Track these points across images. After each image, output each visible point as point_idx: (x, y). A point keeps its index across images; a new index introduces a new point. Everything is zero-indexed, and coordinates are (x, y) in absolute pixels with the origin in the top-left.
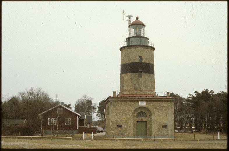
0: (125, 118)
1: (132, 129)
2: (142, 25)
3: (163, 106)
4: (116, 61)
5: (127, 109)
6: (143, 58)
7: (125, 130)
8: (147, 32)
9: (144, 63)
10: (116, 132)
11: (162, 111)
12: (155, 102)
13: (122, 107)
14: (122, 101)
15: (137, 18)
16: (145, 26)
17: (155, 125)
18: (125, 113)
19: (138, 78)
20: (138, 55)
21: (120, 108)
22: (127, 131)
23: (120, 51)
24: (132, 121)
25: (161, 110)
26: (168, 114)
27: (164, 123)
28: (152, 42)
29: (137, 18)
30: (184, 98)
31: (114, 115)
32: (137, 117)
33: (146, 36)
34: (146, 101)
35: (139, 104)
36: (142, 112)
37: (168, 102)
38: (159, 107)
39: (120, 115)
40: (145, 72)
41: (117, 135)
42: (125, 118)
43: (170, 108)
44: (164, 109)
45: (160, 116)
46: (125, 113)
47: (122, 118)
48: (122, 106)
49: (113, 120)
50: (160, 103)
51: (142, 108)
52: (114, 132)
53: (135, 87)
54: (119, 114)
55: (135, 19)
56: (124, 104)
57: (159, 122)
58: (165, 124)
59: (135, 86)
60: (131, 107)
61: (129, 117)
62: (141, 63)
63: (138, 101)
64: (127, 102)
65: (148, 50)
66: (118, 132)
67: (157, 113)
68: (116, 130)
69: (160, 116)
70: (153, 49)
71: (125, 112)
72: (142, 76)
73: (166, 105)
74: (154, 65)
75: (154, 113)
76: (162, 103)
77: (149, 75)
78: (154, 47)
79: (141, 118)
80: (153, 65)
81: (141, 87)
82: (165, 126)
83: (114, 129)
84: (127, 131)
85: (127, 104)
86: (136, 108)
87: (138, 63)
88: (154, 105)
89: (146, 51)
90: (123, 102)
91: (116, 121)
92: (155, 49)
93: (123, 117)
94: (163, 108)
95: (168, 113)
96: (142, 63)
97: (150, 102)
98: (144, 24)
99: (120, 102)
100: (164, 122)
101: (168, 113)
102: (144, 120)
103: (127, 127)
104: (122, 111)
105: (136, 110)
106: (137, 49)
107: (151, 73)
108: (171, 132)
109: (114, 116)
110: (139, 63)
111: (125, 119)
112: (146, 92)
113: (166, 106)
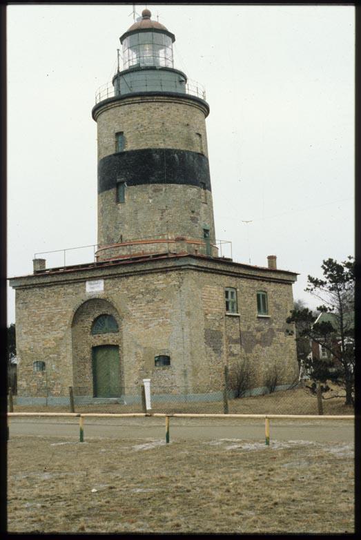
1: (71, 374)
6: (127, 136)
7: (52, 377)
9: (132, 151)
10: (31, 384)
11: (151, 307)
12: (131, 279)
14: (44, 287)
16: (172, 37)
17: (133, 359)
19: (114, 203)
20: (113, 131)
22: (58, 381)
24: (70, 347)
25: (148, 302)
26: (171, 314)
27: (160, 347)
28: (200, 87)
31: (25, 333)
32: (92, 333)
33: (177, 67)
34: (104, 277)
36: (104, 315)
37: (170, 273)
38: (142, 293)
40: (133, 182)
41: (36, 395)
43: (175, 293)
44: (155, 300)
45: (146, 326)
47: (43, 340)
48: (43, 302)
49: (23, 349)
50: (144, 281)
51: (94, 302)
52: (27, 384)
54: (36, 329)
57: (144, 345)
58: (163, 354)
60: (66, 301)
61: (61, 335)
62: (122, 154)
63: (84, 280)
64: (56, 289)
65: (147, 105)
66: (36, 384)
67: (138, 315)
68: (33, 378)
69: (146, 326)
70: (204, 108)
71: (50, 320)
72: (125, 197)
73: (164, 286)
75: (129, 315)
76: (150, 278)
77: (150, 187)
78: (208, 101)
79: (104, 335)
80: (202, 158)
81: (121, 233)
82: (165, 360)
83: (26, 375)
84: (58, 381)
85: (55, 292)
86: (80, 302)
87: (153, 159)
88: (127, 289)
89: (139, 112)
90: (45, 289)
91: (30, 349)
93: (48, 337)
94: (155, 296)
95: (171, 311)
96: (124, 152)
99: (37, 289)
100: (161, 345)
101: (171, 311)
102: (111, 342)
103: (58, 367)
104: (43, 319)
105: (79, 313)
106: (112, 111)
107: (193, 182)
108: (183, 379)
110: (115, 155)
111: (52, 344)
112: (137, 246)
113: (161, 287)
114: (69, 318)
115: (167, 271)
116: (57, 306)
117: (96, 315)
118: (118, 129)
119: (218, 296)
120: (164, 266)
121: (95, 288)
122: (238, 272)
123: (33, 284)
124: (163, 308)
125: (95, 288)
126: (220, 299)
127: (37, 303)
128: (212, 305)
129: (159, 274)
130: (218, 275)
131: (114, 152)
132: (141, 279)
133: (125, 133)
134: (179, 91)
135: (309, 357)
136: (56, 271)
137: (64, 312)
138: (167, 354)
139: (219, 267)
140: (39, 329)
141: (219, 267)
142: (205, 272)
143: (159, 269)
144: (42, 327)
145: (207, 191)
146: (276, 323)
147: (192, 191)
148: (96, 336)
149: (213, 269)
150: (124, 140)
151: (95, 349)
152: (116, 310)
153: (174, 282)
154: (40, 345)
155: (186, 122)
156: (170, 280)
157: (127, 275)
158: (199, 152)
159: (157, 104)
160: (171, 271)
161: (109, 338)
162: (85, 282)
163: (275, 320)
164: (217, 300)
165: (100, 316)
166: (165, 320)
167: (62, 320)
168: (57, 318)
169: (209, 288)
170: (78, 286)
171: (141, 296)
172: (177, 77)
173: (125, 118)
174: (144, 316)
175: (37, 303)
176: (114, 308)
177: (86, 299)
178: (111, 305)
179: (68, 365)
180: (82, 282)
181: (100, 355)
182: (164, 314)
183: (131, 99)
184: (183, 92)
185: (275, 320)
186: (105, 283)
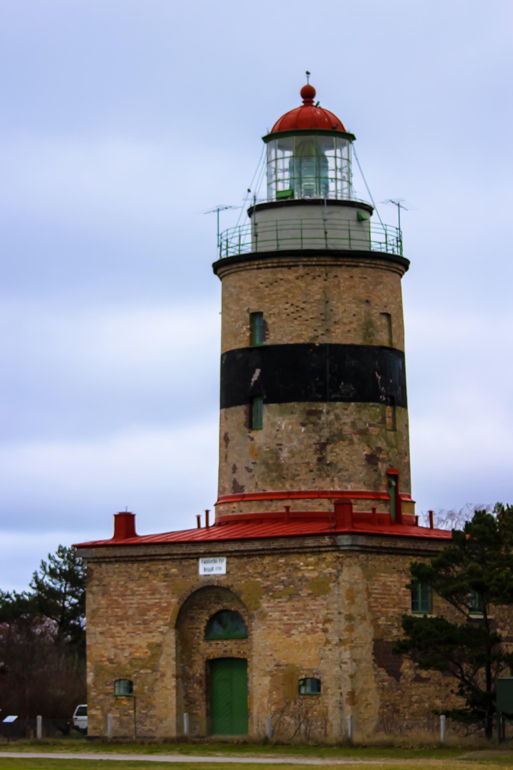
0: (142, 641)
2: (335, 132)
3: (300, 574)
4: (191, 334)
5: (150, 602)
6: (269, 321)
8: (363, 173)
13: (133, 593)
15: (308, 94)
18: (145, 622)
21: (123, 595)
23: (216, 278)
27: (307, 665)
29: (308, 94)
30: (74, 546)
31: (102, 633)
34: (228, 554)
35: (197, 572)
37: (324, 555)
38: (282, 582)
39: (123, 633)
42: (144, 645)
46: (145, 622)
47: (131, 646)
51: (211, 589)
53: (235, 482)
54: (119, 629)
55: (298, 102)
56: (140, 577)
59: (235, 476)
61: (157, 639)
63: (197, 556)
67: (276, 615)
69: (288, 633)
70: (399, 264)
74: (401, 355)
75: (263, 616)
78: (405, 255)
92: (407, 268)
93: (137, 641)
97: (245, 560)
98: (348, 128)
109: (101, 639)
114: (170, 613)
115: (320, 552)
116: (153, 594)
117: (213, 611)
118: (254, 307)
119: (399, 589)
120: (316, 544)
121: (212, 568)
122: (435, 549)
123: (115, 557)
124: (313, 608)
125: (212, 568)
126: (401, 593)
127: (122, 586)
128: (388, 603)
129: (308, 555)
130: (399, 557)
131: (244, 344)
132: (282, 560)
133: (265, 314)
134: (357, 246)
135: (51, 599)
136: (152, 543)
137: (166, 605)
138: (316, 676)
139: (400, 544)
140: (123, 629)
141: (400, 544)
142: (379, 553)
143: (308, 547)
144: (130, 627)
145: (399, 408)
146: (502, 629)
147: (368, 414)
148: (214, 642)
149: (390, 548)
150: (264, 327)
151: (212, 664)
152: (244, 606)
153: (330, 570)
154: (126, 654)
155: (364, 297)
156: (324, 565)
157: (261, 554)
158: (386, 344)
159: (317, 269)
160: (326, 551)
161: (229, 648)
162: (198, 559)
163: (501, 624)
164: (397, 594)
165: (212, 613)
166: (315, 625)
167: (160, 616)
168: (152, 613)
169: (384, 577)
170: (186, 563)
171: (282, 587)
172: (351, 213)
173: (267, 291)
174: (285, 618)
175: (122, 586)
176: (240, 601)
177: (198, 585)
178: (236, 597)
179: (169, 687)
180: (193, 558)
181: (221, 674)
182: (314, 614)
183: (276, 260)
184: (367, 249)
185: (501, 624)
186: (227, 563)
